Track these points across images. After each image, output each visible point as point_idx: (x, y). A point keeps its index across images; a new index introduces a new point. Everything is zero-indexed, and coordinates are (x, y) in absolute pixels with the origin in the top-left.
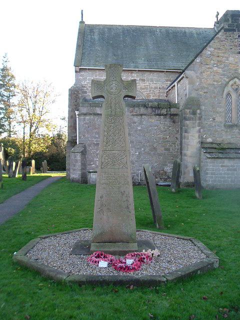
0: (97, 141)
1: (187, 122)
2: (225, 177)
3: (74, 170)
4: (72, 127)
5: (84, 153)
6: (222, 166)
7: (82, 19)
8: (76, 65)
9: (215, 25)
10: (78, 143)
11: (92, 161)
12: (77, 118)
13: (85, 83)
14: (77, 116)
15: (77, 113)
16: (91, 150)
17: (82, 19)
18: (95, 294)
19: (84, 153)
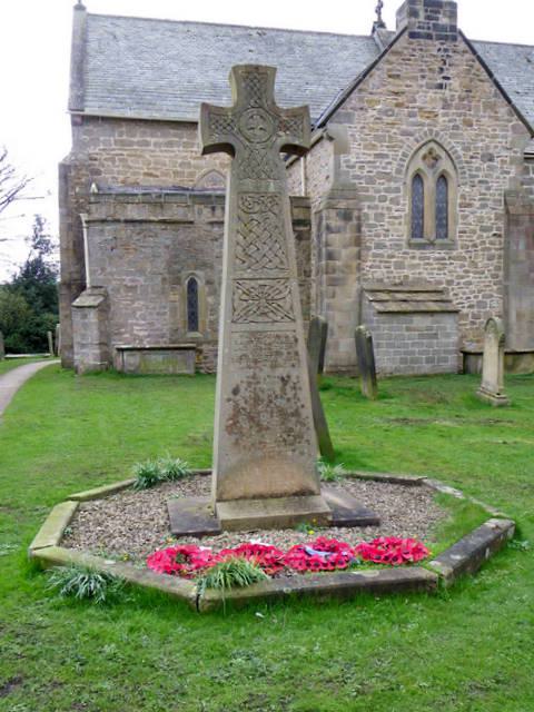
0: (133, 281)
1: (333, 235)
2: (413, 353)
3: (83, 346)
4: (74, 249)
5: (104, 309)
6: (408, 329)
7: (379, 18)
8: (73, 107)
9: (374, 30)
10: (88, 286)
11: (122, 326)
12: (85, 230)
13: (97, 151)
14: (84, 225)
15: (84, 217)
16: (121, 302)
17: (379, 18)
18: (353, 395)
19: (104, 309)
